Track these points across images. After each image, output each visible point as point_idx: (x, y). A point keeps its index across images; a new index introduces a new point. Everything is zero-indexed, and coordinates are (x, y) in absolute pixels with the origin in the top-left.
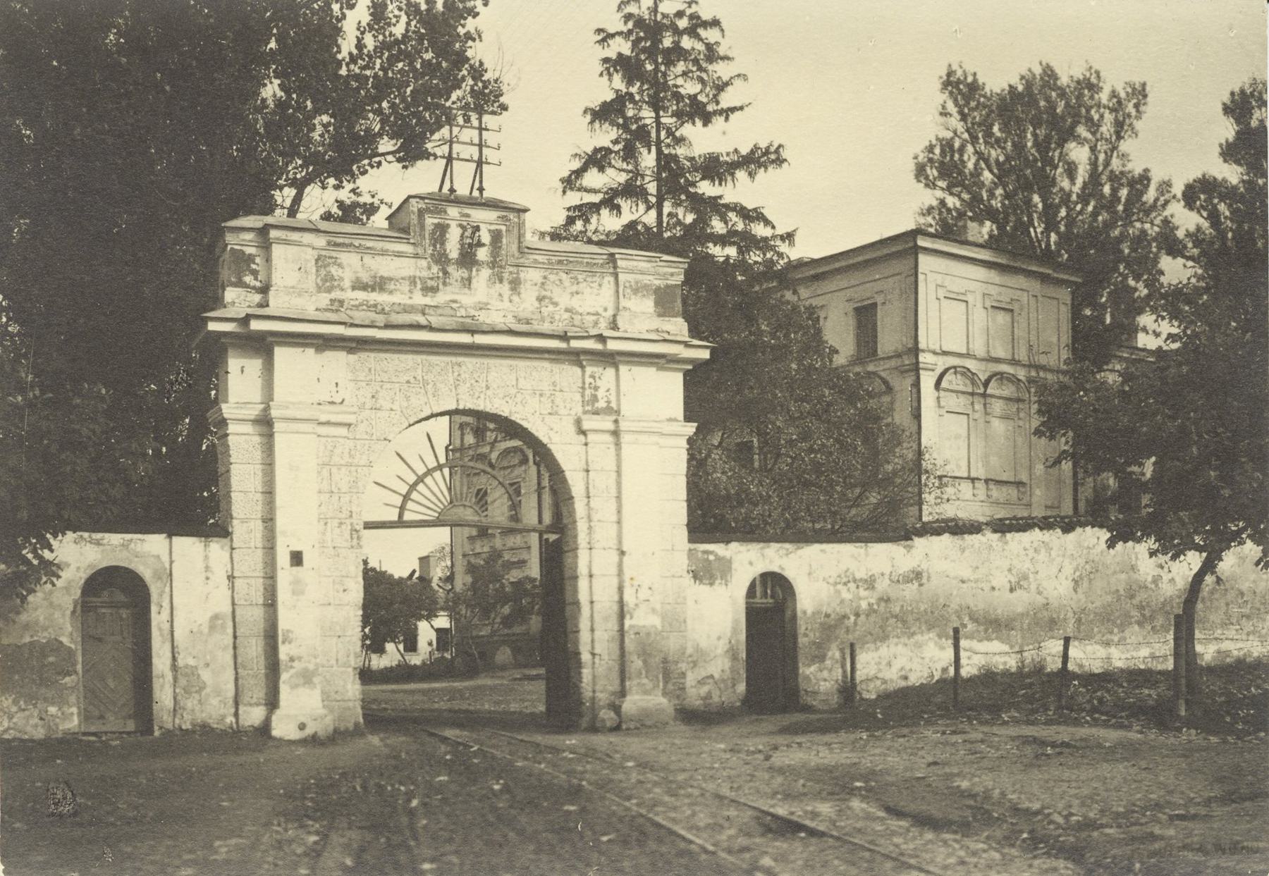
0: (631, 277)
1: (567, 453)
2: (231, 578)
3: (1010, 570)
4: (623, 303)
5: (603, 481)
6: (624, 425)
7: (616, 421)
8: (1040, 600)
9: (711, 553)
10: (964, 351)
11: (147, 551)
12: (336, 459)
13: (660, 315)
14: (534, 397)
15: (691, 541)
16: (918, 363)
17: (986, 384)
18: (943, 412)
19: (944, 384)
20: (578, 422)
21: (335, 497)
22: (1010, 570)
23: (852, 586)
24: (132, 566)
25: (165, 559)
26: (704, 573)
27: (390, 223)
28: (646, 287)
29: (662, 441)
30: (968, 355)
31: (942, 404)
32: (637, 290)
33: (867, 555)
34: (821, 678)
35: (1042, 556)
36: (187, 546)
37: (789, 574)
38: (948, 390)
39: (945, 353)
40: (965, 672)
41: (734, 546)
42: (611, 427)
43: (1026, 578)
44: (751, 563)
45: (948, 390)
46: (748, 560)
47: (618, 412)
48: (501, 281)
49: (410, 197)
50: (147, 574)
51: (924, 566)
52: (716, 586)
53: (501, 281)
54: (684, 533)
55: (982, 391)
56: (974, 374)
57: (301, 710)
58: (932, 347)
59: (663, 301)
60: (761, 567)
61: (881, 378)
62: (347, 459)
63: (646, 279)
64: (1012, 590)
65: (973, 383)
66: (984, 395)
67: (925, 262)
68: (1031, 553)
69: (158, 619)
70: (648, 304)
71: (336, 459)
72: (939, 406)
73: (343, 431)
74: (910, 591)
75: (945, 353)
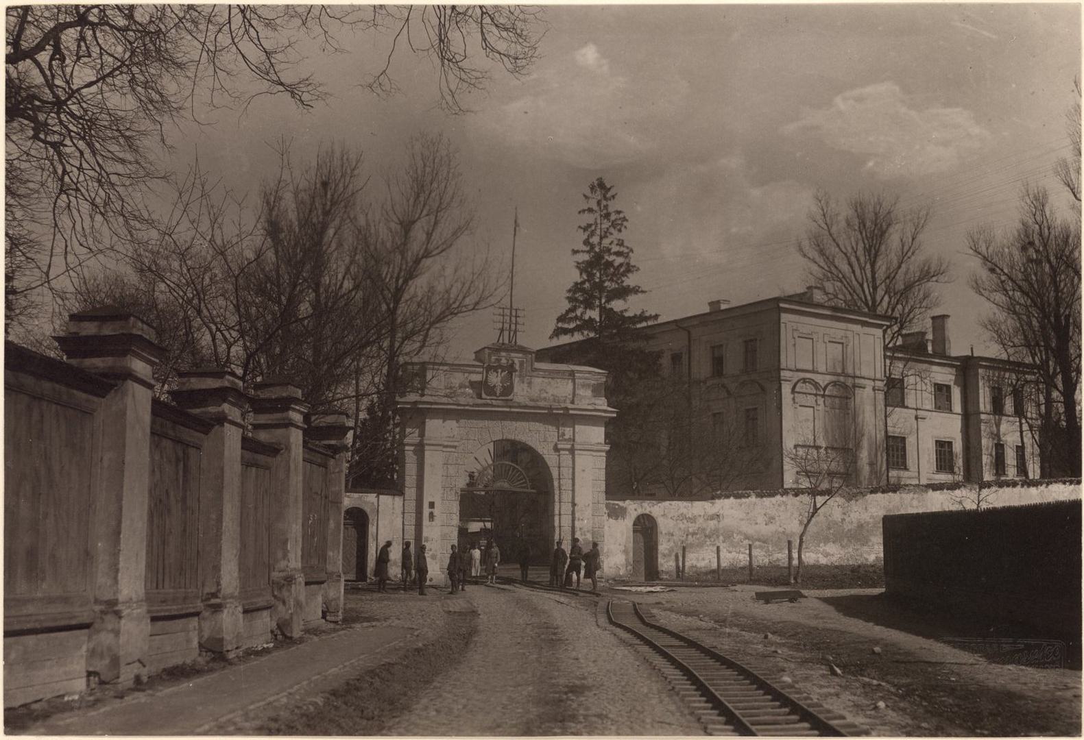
0: (582, 381)
1: (551, 459)
2: (403, 513)
3: (765, 515)
4: (577, 392)
5: (566, 472)
6: (576, 447)
7: (573, 445)
8: (781, 530)
9: (617, 504)
10: (811, 368)
11: (368, 500)
12: (450, 462)
13: (595, 397)
14: (539, 437)
15: (607, 499)
16: (780, 376)
17: (824, 390)
18: (797, 406)
19: (797, 389)
20: (556, 445)
21: (449, 479)
22: (765, 515)
23: (685, 521)
24: (362, 507)
25: (376, 504)
26: (616, 513)
27: (476, 356)
28: (588, 385)
29: (594, 454)
30: (813, 372)
31: (796, 400)
32: (583, 386)
33: (692, 506)
34: (666, 564)
35: (783, 508)
36: (385, 500)
37: (654, 514)
38: (799, 393)
39: (798, 370)
40: (724, 564)
41: (628, 502)
42: (569, 447)
43: (774, 518)
44: (636, 510)
45: (799, 393)
46: (634, 508)
47: (574, 440)
48: (523, 382)
49: (485, 348)
50: (367, 509)
51: (721, 512)
52: (619, 520)
53: (523, 382)
54: (604, 495)
55: (822, 393)
56: (816, 383)
57: (313, 425)
58: (790, 367)
59: (596, 391)
60: (640, 511)
61: (759, 384)
62: (455, 462)
63: (588, 382)
64: (766, 524)
65: (817, 388)
66: (823, 396)
67: (785, 317)
68: (776, 507)
69: (372, 529)
70: (589, 393)
71: (450, 462)
72: (794, 403)
73: (453, 450)
74: (712, 524)
75: (798, 370)
